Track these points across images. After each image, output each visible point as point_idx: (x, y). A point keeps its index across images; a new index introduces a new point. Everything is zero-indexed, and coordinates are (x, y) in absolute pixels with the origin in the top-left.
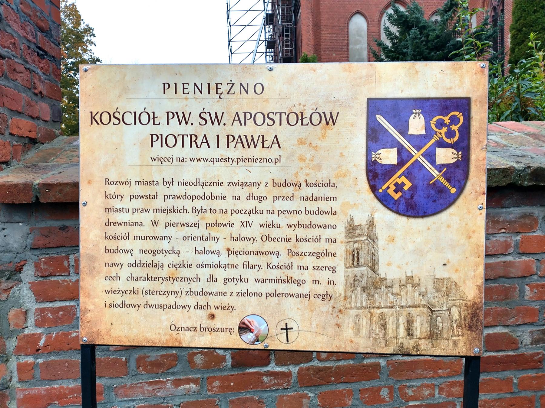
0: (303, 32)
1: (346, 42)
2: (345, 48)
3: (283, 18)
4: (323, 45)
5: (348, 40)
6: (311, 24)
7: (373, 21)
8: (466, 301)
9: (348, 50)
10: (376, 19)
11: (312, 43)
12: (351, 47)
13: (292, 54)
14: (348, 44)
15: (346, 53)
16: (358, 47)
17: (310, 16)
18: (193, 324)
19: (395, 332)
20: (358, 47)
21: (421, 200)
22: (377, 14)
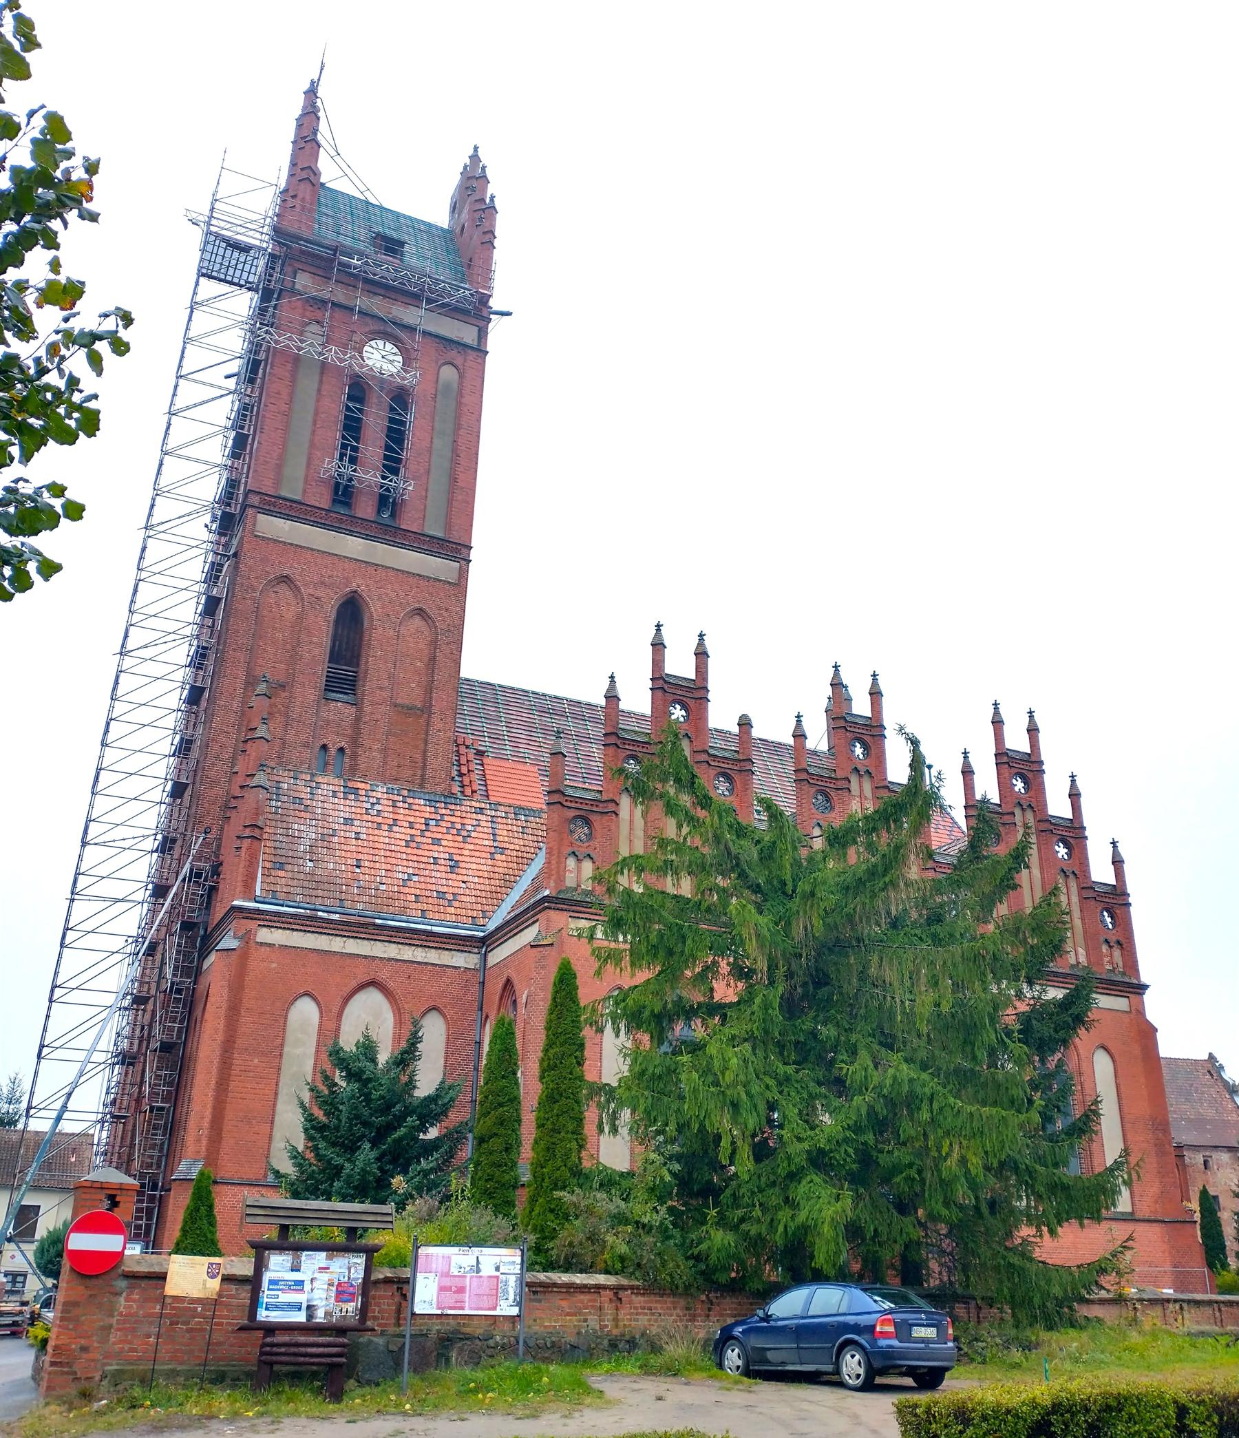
0: (201, 1055)
1: (279, 1041)
2: (277, 1052)
3: (176, 968)
4: (239, 1041)
5: (283, 1039)
6: (224, 1005)
7: (330, 1011)
8: (27, 1116)
9: (281, 1055)
10: (335, 1009)
11: (220, 1037)
12: (286, 1049)
13: (179, 1037)
14: (282, 1045)
15: (277, 1060)
16: (299, 1051)
17: (225, 992)
18: (535, 761)
19: (130, 1193)
20: (299, 1051)
21: (213, 1277)
22: (339, 1001)
